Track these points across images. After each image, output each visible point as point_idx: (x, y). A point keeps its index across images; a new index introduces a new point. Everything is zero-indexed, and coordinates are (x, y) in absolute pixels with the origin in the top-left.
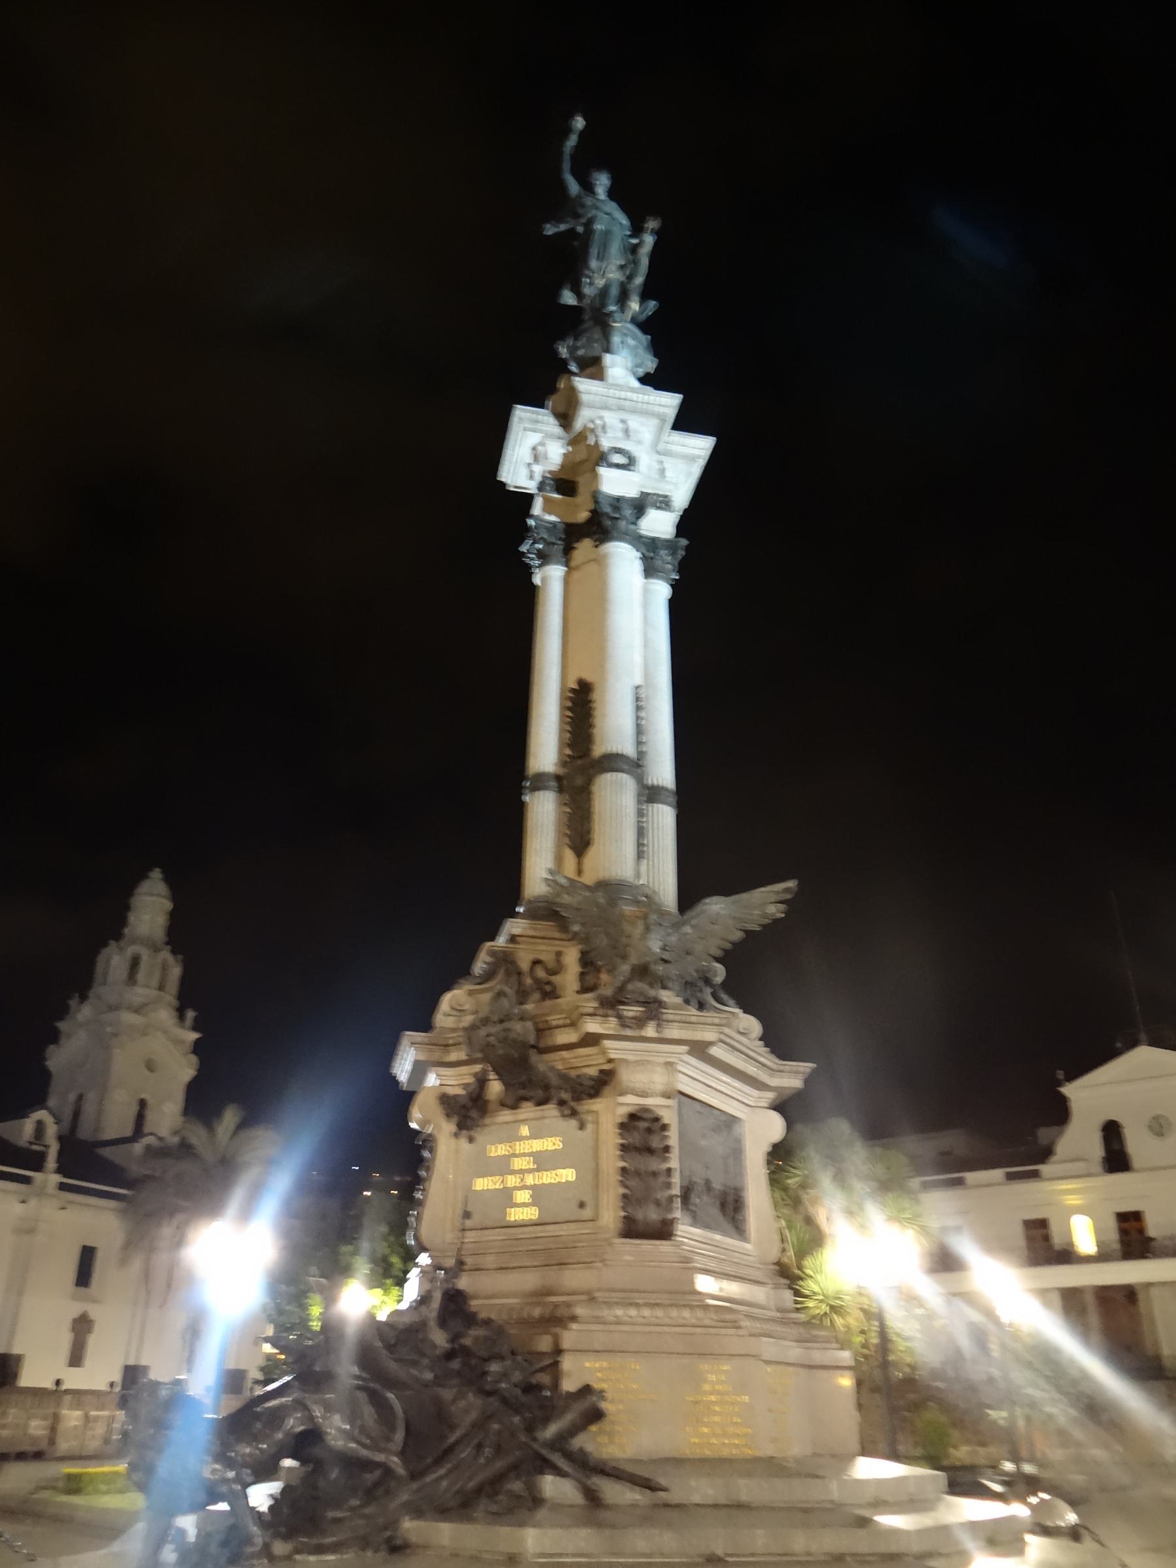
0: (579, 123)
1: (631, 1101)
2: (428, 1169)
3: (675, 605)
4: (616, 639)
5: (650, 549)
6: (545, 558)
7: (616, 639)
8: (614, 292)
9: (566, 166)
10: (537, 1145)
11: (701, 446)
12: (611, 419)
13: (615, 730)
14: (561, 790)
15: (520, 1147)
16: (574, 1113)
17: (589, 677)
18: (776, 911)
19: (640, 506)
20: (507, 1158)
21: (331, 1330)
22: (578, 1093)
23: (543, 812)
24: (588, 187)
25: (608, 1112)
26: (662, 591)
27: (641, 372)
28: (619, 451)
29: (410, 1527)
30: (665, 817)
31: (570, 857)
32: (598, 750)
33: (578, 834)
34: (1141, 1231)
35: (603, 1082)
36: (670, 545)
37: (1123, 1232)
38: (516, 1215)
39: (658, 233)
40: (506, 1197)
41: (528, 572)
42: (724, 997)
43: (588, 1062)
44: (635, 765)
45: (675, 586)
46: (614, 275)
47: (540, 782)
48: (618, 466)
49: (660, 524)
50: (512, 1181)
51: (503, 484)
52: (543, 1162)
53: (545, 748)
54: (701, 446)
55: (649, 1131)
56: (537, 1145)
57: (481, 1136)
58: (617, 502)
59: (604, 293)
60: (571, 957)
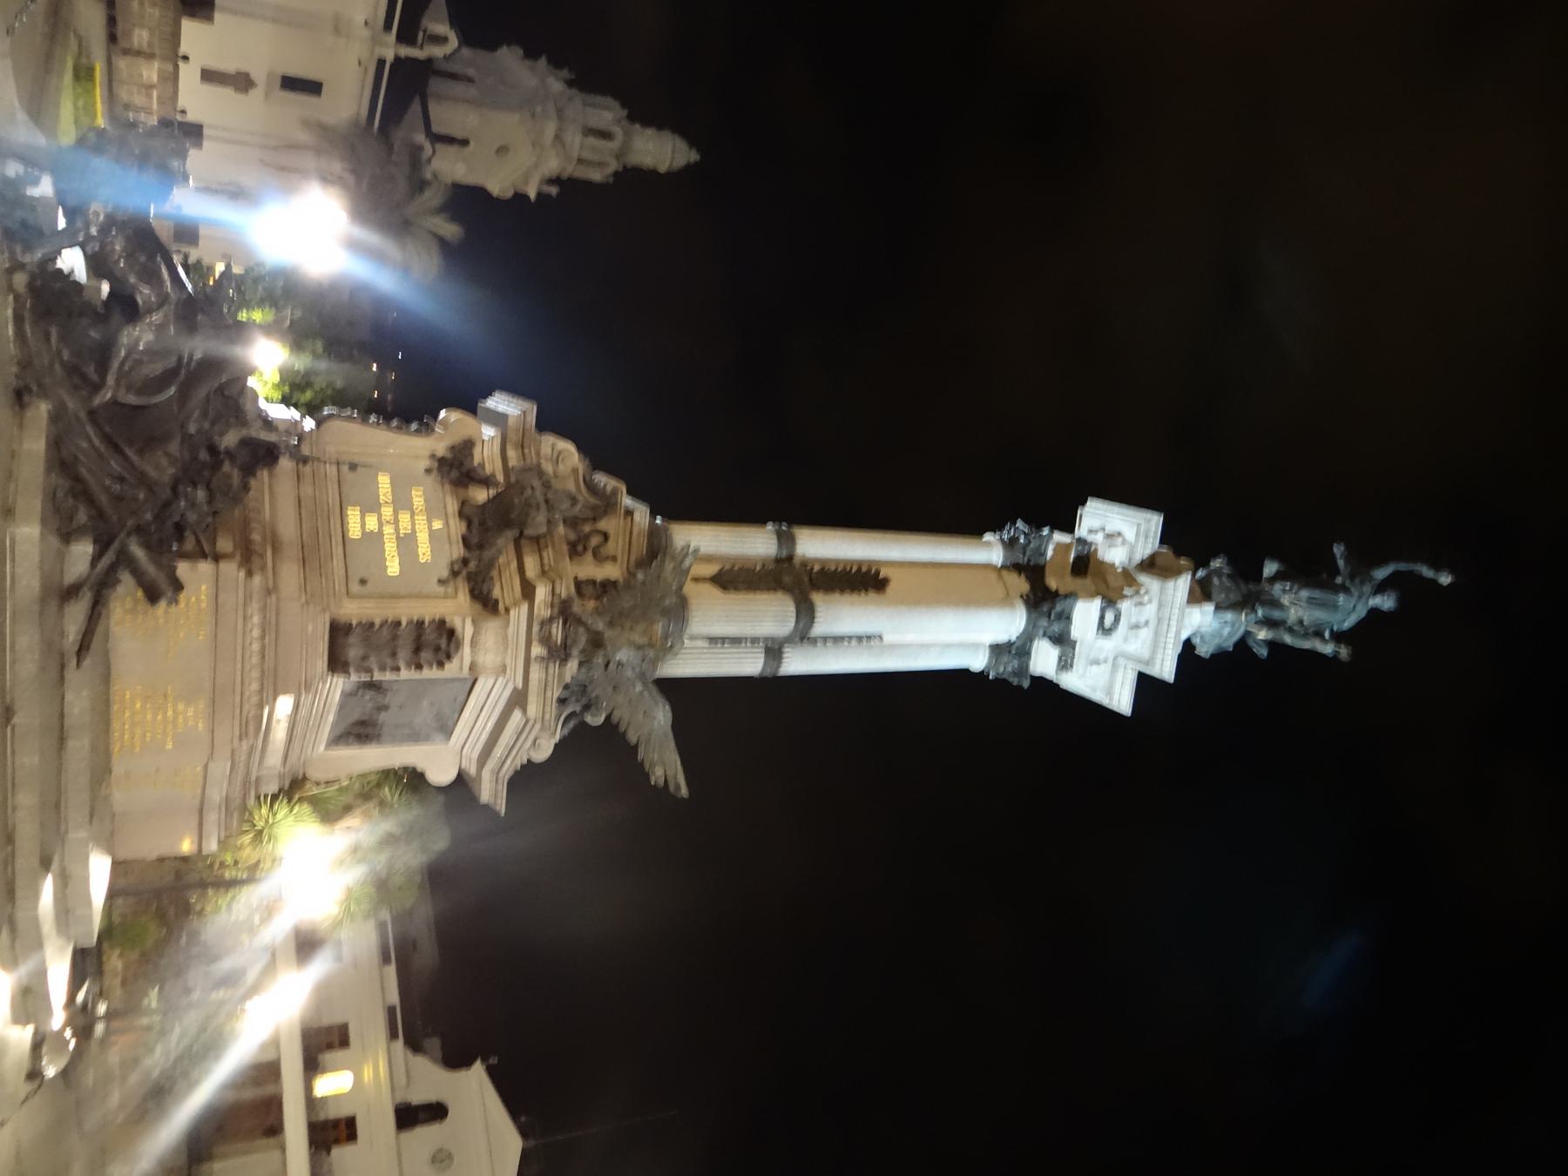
0: (1445, 579)
2: (399, 428)
3: (961, 676)
4: (928, 616)
5: (1018, 650)
6: (1010, 544)
7: (928, 616)
9: (1402, 567)
10: (423, 537)
11: (1122, 700)
12: (1150, 611)
13: (839, 615)
14: (778, 561)
15: (421, 520)
16: (455, 574)
18: (657, 776)
19: (1062, 640)
20: (409, 507)
21: (239, 331)
22: (475, 577)
24: (1380, 588)
25: (456, 608)
26: (977, 662)
27: (1196, 641)
28: (1117, 619)
30: (750, 665)
31: (711, 570)
32: (818, 598)
33: (735, 578)
35: (486, 603)
36: (1023, 670)
38: (353, 515)
40: (372, 506)
41: (996, 527)
42: (571, 724)
44: (803, 635)
45: (982, 675)
46: (1293, 614)
47: (786, 540)
48: (1102, 618)
49: (1044, 660)
51: (1084, 503)
52: (407, 543)
53: (821, 545)
54: (1122, 700)
55: (437, 649)
56: (423, 537)
57: (432, 481)
58: (1066, 617)
59: (1275, 604)
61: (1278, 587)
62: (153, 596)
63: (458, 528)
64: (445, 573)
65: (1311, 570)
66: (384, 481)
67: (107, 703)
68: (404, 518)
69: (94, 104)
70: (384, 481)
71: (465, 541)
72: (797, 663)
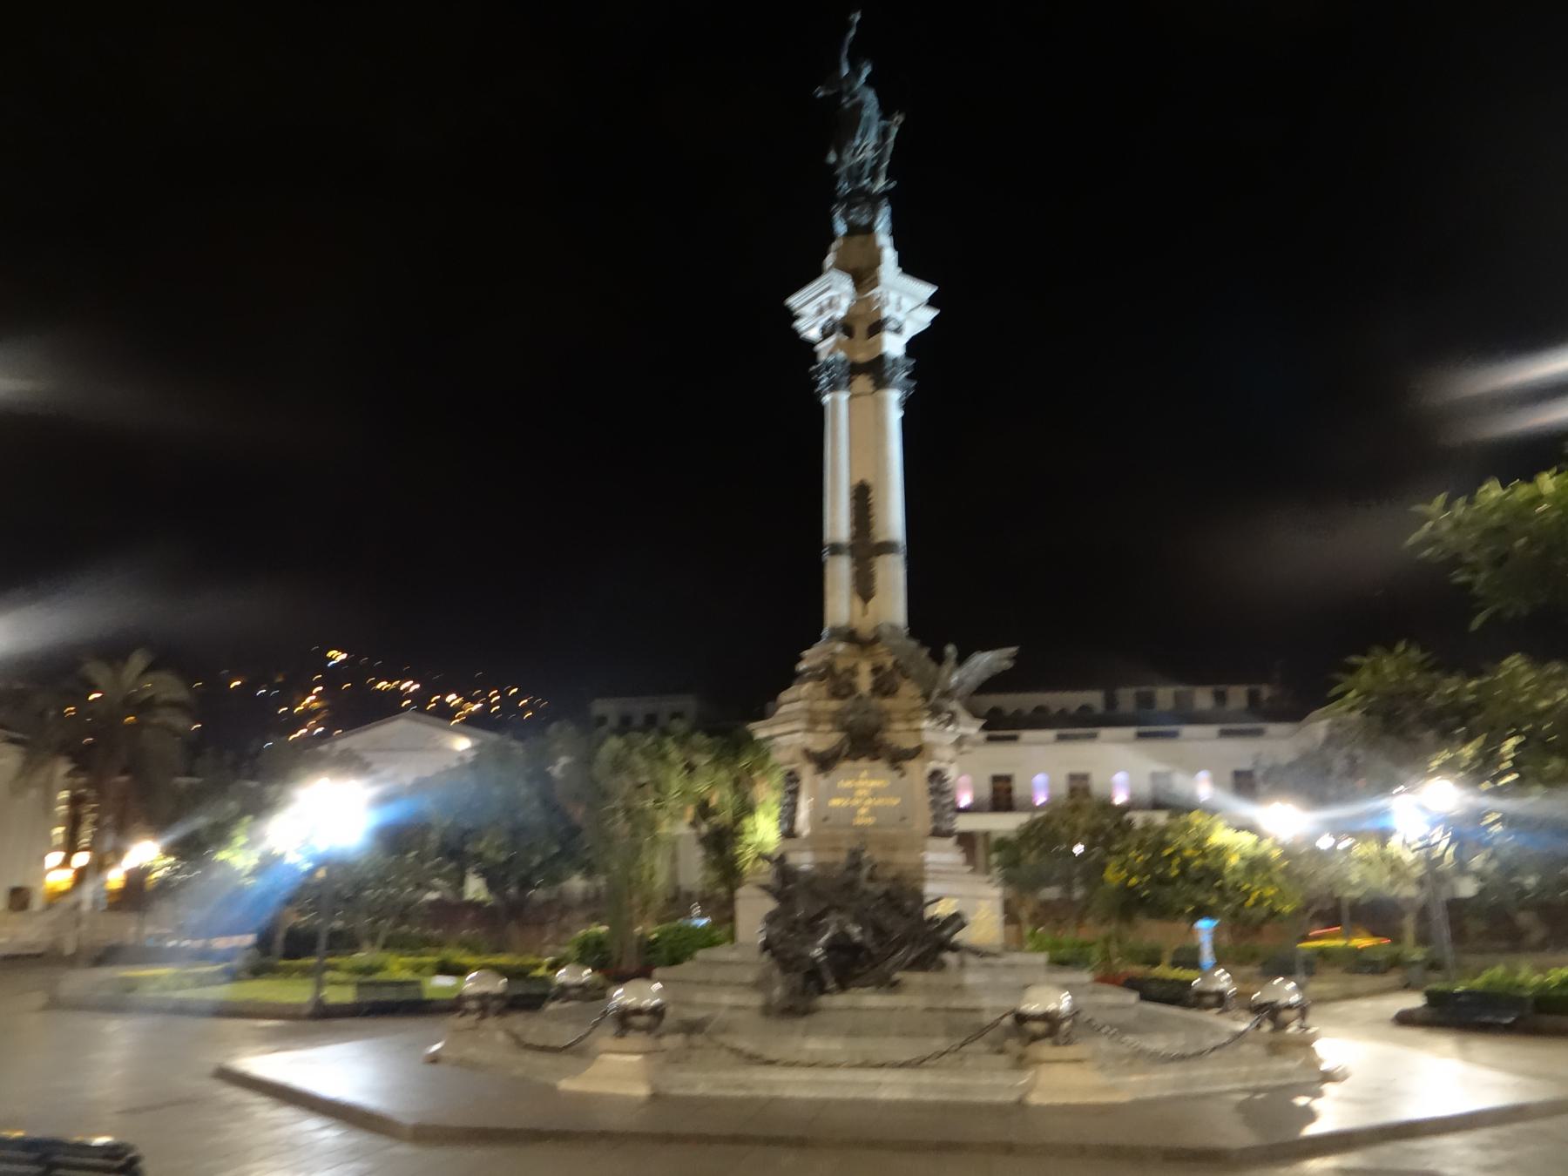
0: (857, 17)
1: (932, 765)
4: (866, 449)
6: (834, 386)
7: (866, 449)
8: (867, 167)
9: (845, 52)
10: (873, 783)
12: (893, 297)
14: (852, 555)
15: (861, 783)
16: (897, 768)
17: (870, 480)
18: (1007, 664)
20: (854, 789)
21: (168, 852)
22: (898, 758)
23: (839, 573)
24: (855, 72)
25: (917, 771)
29: (898, 975)
30: (893, 574)
31: (858, 603)
32: (881, 538)
33: (864, 588)
34: (1009, 790)
35: (917, 752)
37: (995, 790)
38: (859, 821)
39: (902, 128)
40: (853, 811)
43: (909, 743)
46: (869, 154)
47: (836, 549)
50: (856, 802)
52: (875, 793)
53: (838, 523)
56: (873, 783)
57: (833, 775)
59: (862, 164)
60: (865, 668)
61: (847, 156)
62: (963, 926)
63: (863, 763)
64: (896, 774)
65: (843, 125)
66: (835, 802)
67: (29, 956)
68: (860, 793)
69: (155, 978)
70: (835, 802)
71: (875, 758)
72: (893, 519)
